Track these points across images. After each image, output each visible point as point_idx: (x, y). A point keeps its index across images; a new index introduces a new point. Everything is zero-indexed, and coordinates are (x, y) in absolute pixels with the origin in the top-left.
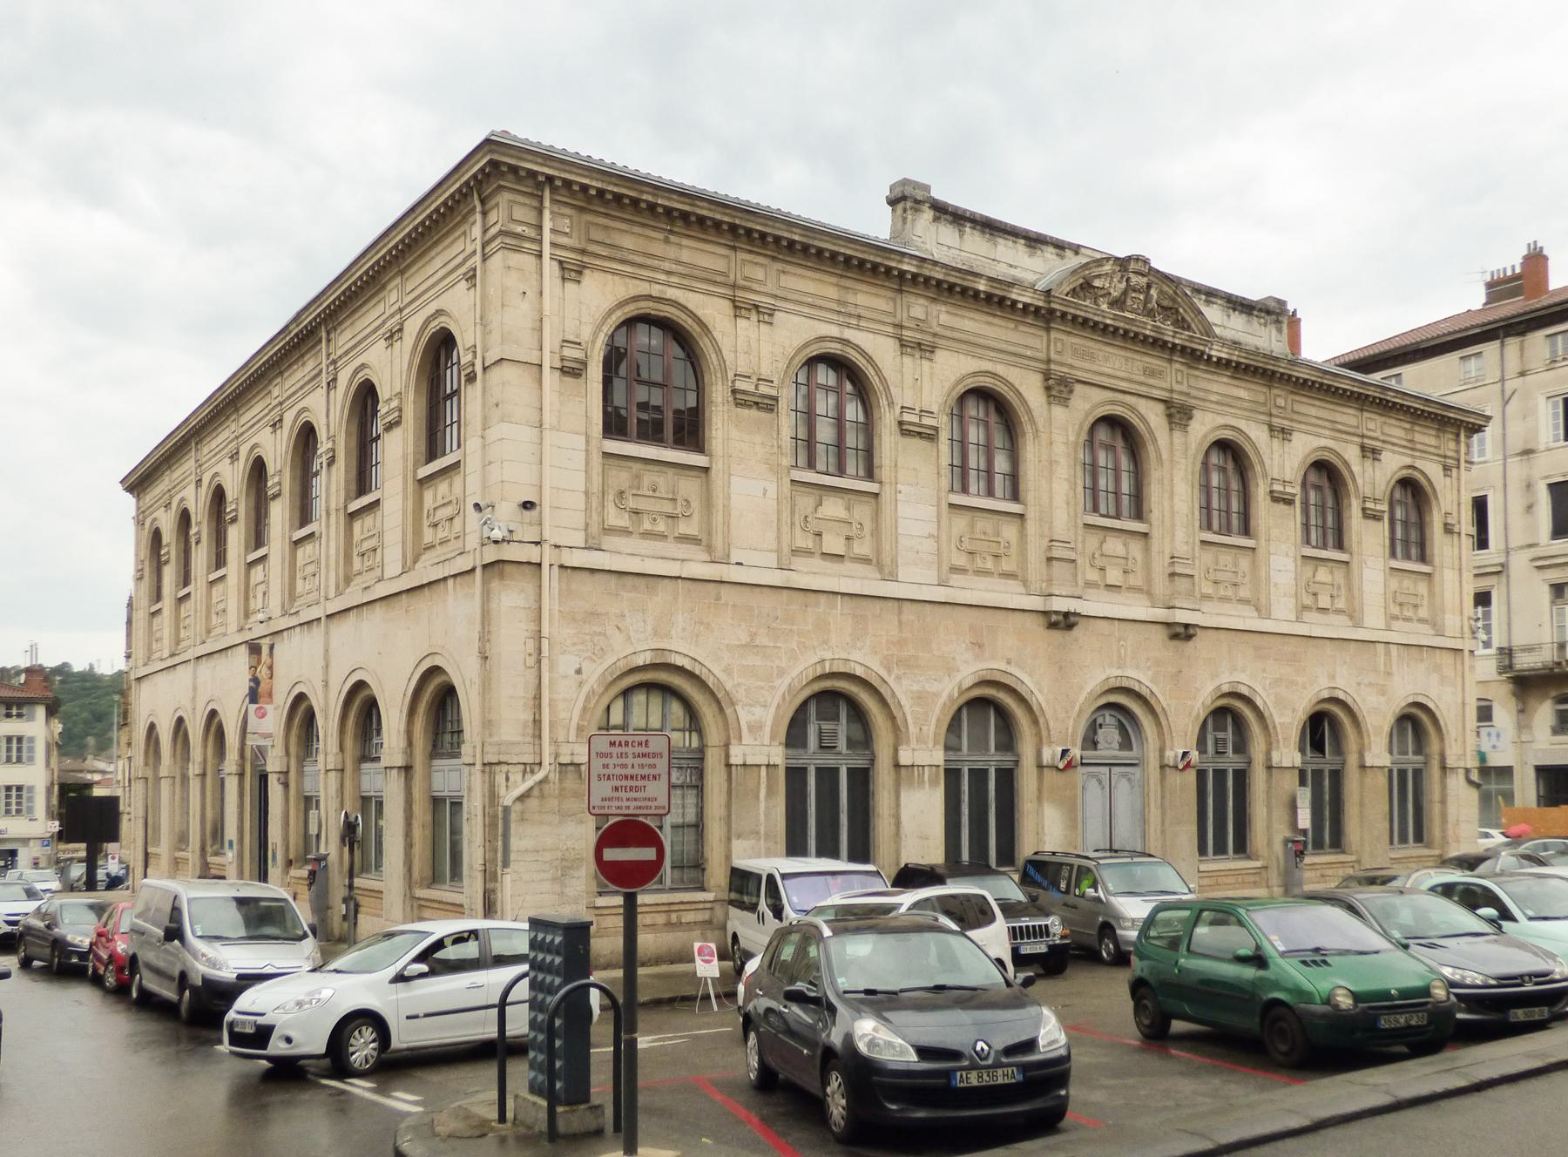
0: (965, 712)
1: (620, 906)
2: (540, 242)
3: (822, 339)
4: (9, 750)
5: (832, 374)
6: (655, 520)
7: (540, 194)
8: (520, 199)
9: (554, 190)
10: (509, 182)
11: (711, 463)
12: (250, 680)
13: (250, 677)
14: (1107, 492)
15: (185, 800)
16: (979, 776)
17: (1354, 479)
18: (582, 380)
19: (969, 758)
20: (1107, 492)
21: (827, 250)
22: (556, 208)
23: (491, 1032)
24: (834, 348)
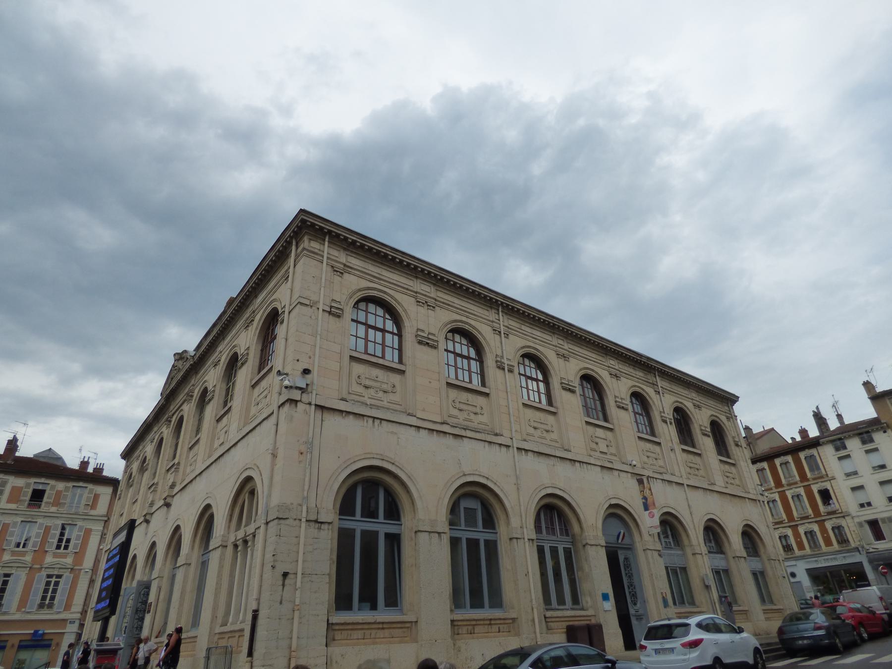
1: (183, 643)
3: (456, 321)
6: (377, 391)
9: (503, 307)
12: (642, 499)
14: (375, 342)
15: (678, 580)
19: (359, 524)
20: (375, 342)
24: (460, 325)
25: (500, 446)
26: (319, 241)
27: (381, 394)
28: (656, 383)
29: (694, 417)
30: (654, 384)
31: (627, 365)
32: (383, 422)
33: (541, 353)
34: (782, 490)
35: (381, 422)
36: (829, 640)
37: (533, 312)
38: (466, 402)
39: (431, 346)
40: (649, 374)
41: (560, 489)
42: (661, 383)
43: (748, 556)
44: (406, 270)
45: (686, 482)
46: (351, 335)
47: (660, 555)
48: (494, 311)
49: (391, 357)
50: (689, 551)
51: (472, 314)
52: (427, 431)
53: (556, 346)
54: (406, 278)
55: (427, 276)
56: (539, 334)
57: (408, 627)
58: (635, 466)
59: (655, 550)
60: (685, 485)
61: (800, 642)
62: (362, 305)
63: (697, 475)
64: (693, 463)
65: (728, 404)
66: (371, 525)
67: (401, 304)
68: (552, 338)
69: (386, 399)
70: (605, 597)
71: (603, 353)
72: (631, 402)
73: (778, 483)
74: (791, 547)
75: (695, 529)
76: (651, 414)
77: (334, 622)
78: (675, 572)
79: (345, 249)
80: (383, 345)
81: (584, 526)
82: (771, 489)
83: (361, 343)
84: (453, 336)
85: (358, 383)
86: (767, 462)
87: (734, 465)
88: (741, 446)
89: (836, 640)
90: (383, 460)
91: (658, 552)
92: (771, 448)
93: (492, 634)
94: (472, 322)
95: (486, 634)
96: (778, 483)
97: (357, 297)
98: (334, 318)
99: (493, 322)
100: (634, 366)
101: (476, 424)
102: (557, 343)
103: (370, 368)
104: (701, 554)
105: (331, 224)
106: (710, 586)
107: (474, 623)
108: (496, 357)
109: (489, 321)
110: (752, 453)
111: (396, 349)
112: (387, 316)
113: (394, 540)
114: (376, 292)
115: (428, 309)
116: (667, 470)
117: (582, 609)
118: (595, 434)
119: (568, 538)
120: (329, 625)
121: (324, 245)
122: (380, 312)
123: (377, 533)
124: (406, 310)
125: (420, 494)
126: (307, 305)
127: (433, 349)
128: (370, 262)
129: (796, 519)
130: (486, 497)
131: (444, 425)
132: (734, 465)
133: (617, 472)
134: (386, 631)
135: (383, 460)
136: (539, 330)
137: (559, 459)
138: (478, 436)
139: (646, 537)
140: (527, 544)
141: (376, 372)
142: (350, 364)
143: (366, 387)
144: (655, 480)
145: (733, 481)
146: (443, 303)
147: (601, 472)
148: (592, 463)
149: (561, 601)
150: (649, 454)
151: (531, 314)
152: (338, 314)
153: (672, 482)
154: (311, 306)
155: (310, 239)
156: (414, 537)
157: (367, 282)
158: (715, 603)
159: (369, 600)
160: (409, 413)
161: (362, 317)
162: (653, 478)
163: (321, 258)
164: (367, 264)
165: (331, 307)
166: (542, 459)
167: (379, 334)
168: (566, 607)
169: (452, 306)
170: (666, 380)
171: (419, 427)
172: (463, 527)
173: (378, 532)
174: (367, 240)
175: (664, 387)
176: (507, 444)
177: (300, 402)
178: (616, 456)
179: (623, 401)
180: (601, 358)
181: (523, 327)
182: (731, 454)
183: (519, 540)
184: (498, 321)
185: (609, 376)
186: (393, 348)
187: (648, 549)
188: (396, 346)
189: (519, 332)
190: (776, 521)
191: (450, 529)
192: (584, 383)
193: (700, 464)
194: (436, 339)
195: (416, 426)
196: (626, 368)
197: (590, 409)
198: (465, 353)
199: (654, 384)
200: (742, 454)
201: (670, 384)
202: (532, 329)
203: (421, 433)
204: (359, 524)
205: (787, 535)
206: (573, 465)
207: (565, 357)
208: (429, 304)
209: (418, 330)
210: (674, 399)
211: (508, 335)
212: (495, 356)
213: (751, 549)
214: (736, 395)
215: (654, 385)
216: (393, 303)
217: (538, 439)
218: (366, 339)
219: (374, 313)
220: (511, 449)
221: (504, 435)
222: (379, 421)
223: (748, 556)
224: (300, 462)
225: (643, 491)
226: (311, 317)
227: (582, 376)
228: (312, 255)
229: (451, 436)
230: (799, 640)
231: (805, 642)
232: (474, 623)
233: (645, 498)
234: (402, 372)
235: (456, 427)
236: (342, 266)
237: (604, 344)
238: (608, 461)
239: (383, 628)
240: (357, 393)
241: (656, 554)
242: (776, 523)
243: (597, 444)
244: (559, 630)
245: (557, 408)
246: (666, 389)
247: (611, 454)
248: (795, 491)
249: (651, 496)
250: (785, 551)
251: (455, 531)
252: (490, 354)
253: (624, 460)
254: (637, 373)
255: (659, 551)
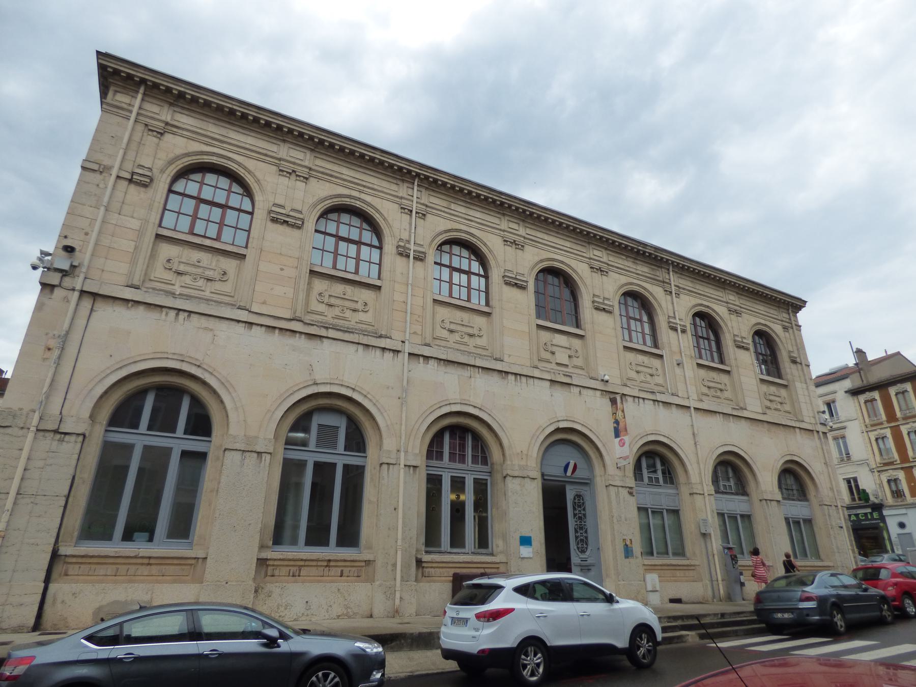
0: (447, 438)
2: (138, 114)
5: (359, 221)
7: (668, 267)
8: (784, 311)
9: (421, 180)
10: (407, 178)
11: (157, 229)
12: (614, 423)
13: (613, 421)
16: (323, 471)
18: (301, 230)
21: (723, 278)
22: (419, 189)
25: (383, 351)
26: (131, 93)
27: (201, 283)
28: (668, 281)
29: (726, 325)
30: (664, 282)
31: (624, 257)
32: (192, 315)
33: (478, 239)
34: (897, 424)
35: (177, 315)
36: (820, 615)
37: (468, 186)
38: (712, 380)
39: (291, 225)
40: (660, 269)
41: (475, 407)
42: (674, 279)
43: (784, 498)
44: (544, 225)
45: (693, 404)
46: (434, 279)
47: (631, 494)
48: (406, 185)
49: (478, 301)
50: (685, 491)
51: (369, 188)
52: (263, 329)
53: (504, 231)
54: (267, 141)
55: (579, 235)
56: (478, 215)
57: (191, 565)
58: (607, 381)
59: (623, 487)
60: (692, 409)
61: (779, 615)
62: (446, 248)
63: (718, 397)
64: (715, 382)
65: (788, 310)
66: (323, 455)
67: (253, 173)
68: (501, 220)
69: (208, 290)
70: (526, 541)
71: (585, 242)
72: (754, 341)
73: (891, 416)
74: (902, 493)
75: (698, 463)
76: (656, 320)
77: (68, 554)
78: (797, 523)
79: (171, 104)
80: (469, 287)
81: (507, 452)
82: (882, 424)
83: (446, 287)
84: (451, 248)
85: (166, 268)
86: (879, 391)
87: (785, 386)
88: (801, 364)
89: (833, 616)
90: (183, 361)
91: (628, 489)
92: (891, 376)
93: (142, 578)
94: (368, 199)
95: (319, 578)
96: (891, 416)
97: (183, 163)
98: (138, 188)
99: (402, 198)
100: (635, 259)
101: (353, 323)
102: (728, 299)
103: (190, 250)
104: (704, 494)
105: (432, 170)
106: (710, 534)
107: (302, 563)
108: (668, 318)
109: (397, 197)
110: (863, 381)
111: (625, 328)
112: (473, 257)
113: (354, 475)
114: (215, 158)
115: (296, 180)
116: (668, 389)
117: (492, 554)
118: (552, 341)
119: (672, 486)
120: (262, 562)
121: (413, 189)
122: (465, 253)
123: (334, 465)
124: (259, 181)
125: (236, 405)
126: (94, 171)
127: (295, 230)
128: (212, 121)
129: (911, 460)
130: (352, 412)
131: (293, 323)
132: (785, 386)
133: (578, 389)
134: (153, 567)
135: (183, 361)
136: (479, 209)
137: (480, 370)
138: (347, 337)
139: (611, 469)
140: (402, 471)
141: (196, 255)
142: (433, 307)
143: (451, 331)
144: (641, 400)
145: (779, 407)
146: (323, 173)
147: (550, 388)
148: (535, 376)
149: (457, 540)
150: (640, 368)
151: (549, 218)
152: (143, 182)
153: (670, 403)
154: (101, 172)
155: (116, 92)
156: (221, 455)
157: (202, 145)
158: (714, 555)
159: (317, 536)
160: (496, 358)
161: (446, 260)
162: (639, 397)
163: (411, 203)
164: (205, 122)
165: (133, 173)
166: (451, 369)
167: (464, 277)
168: (466, 550)
169: (336, 177)
170: (688, 278)
171: (251, 324)
172: (654, 484)
173: (336, 464)
174: (250, 108)
175: (680, 285)
176: (394, 348)
177: (59, 288)
178: (583, 369)
179: (744, 341)
180: (579, 248)
181: (453, 206)
182: (783, 371)
183: (391, 466)
184: (410, 197)
185: (590, 270)
186: (479, 290)
187: (610, 485)
188: (483, 288)
189: (444, 212)
190: (886, 461)
191: (285, 449)
192: (757, 338)
193: (786, 396)
194: (611, 304)
195: (246, 322)
196: (620, 261)
197: (708, 348)
198: (465, 267)
199: (664, 282)
200: (801, 373)
201: (692, 282)
202: (468, 209)
203: (325, 343)
204: (447, 471)
205: (898, 478)
206: (503, 378)
207: (601, 271)
208: (297, 173)
209: (594, 295)
210: (695, 301)
211: (678, 294)
212: (667, 317)
213: (795, 492)
214: (803, 299)
215: (663, 283)
216: (479, 244)
217: (454, 344)
218: (451, 283)
219: (459, 254)
220: (400, 355)
221: (748, 409)
222: (186, 314)
223: (784, 498)
224: (44, 359)
225: (616, 414)
226: (98, 185)
227: (694, 314)
228: (115, 110)
229: (303, 336)
230: (778, 612)
231: (786, 616)
232: (302, 563)
233: (617, 422)
234: (488, 314)
235: (313, 325)
236: (163, 125)
237: (584, 228)
238: (564, 375)
239: (149, 564)
240: (162, 281)
241: (624, 493)
242: (885, 464)
243: (553, 353)
244: (444, 578)
245: (788, 381)
246: (684, 289)
247: (575, 367)
248: (912, 427)
249: (623, 420)
250: (893, 497)
251: (323, 454)
252: (390, 238)
253: (593, 375)
254: (639, 268)
255: (631, 488)
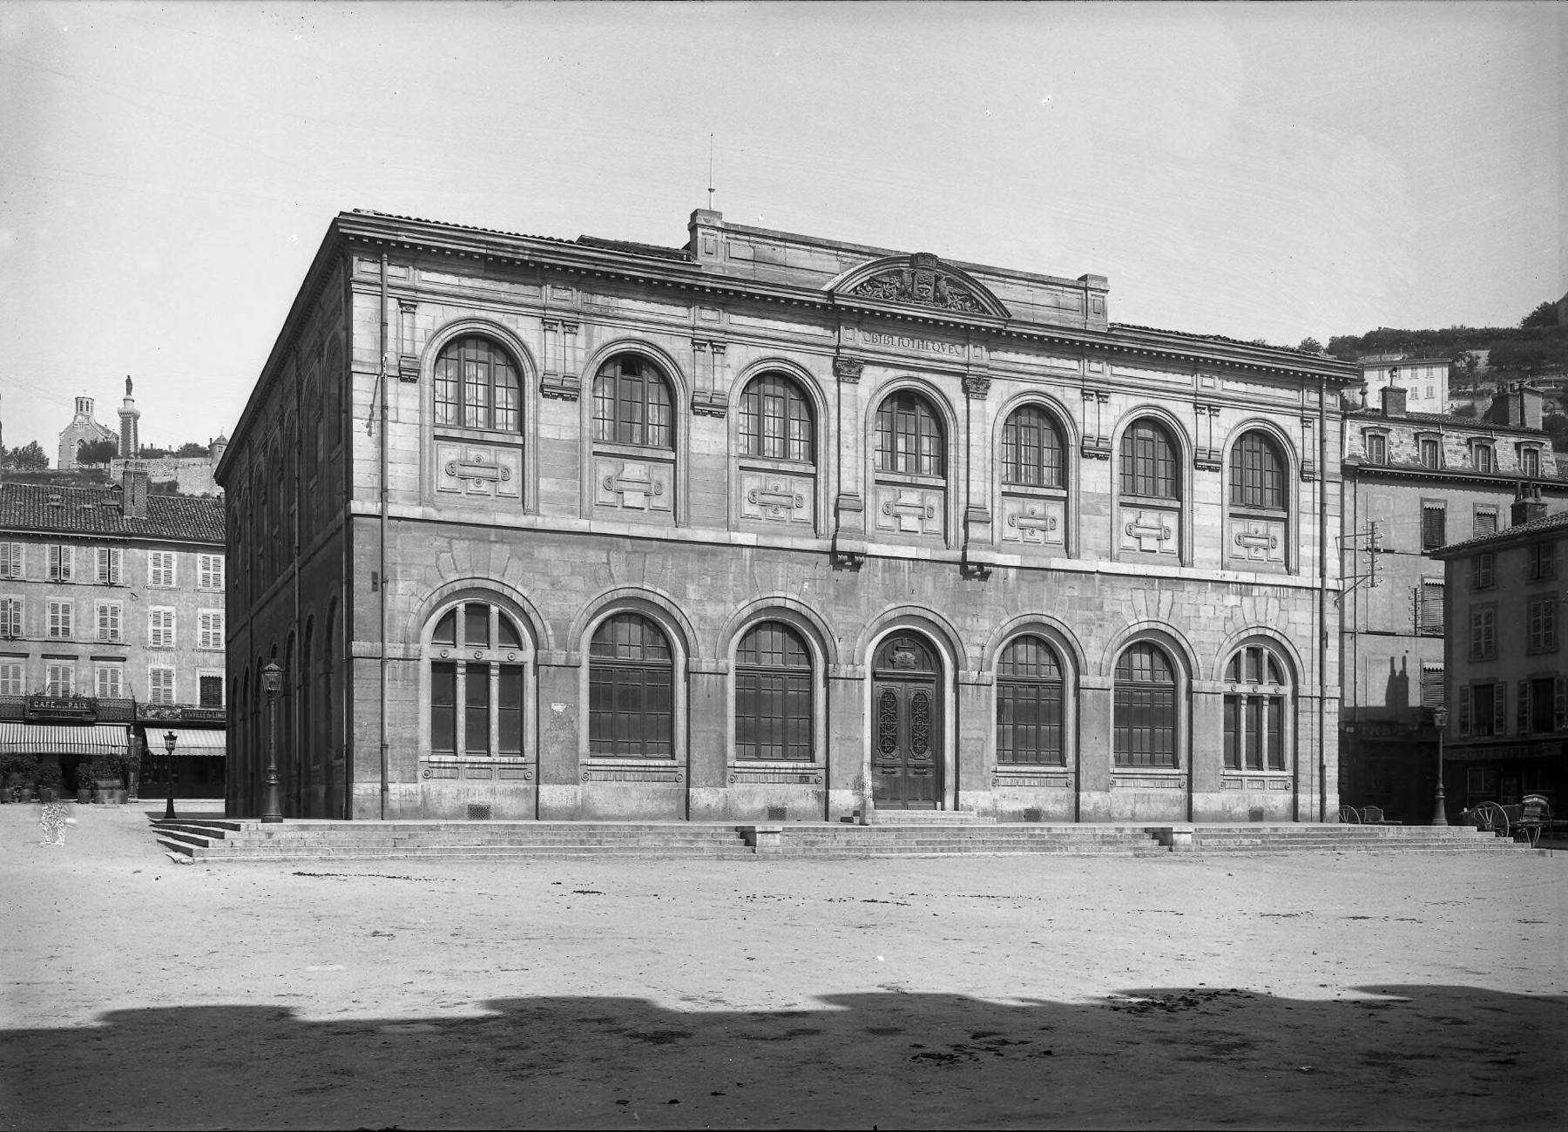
4: (66, 620)
17: (1293, 448)
23: (1337, 701)
